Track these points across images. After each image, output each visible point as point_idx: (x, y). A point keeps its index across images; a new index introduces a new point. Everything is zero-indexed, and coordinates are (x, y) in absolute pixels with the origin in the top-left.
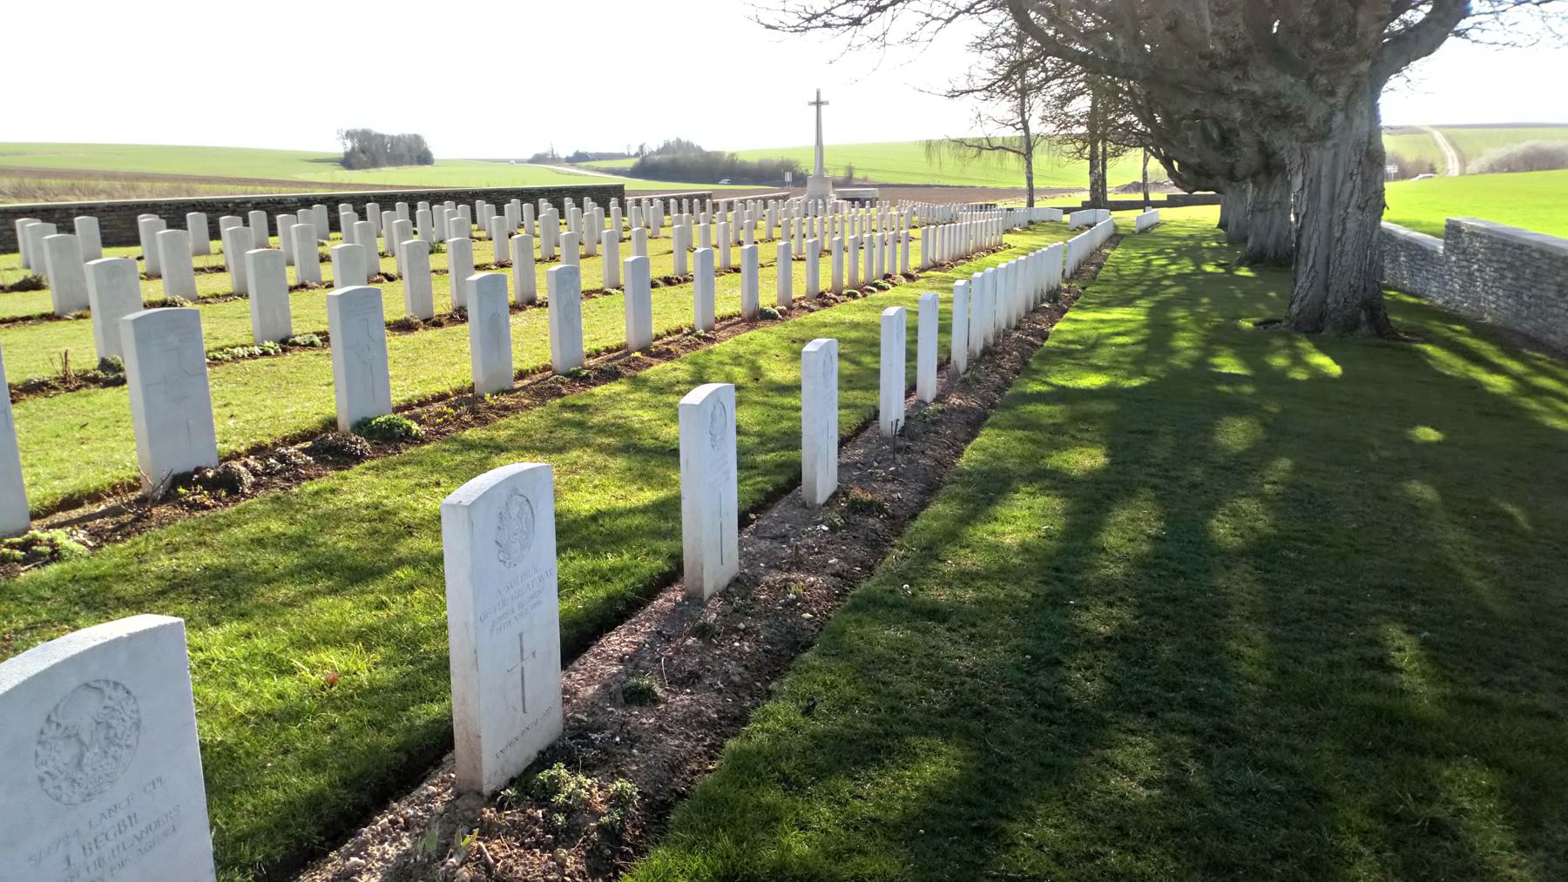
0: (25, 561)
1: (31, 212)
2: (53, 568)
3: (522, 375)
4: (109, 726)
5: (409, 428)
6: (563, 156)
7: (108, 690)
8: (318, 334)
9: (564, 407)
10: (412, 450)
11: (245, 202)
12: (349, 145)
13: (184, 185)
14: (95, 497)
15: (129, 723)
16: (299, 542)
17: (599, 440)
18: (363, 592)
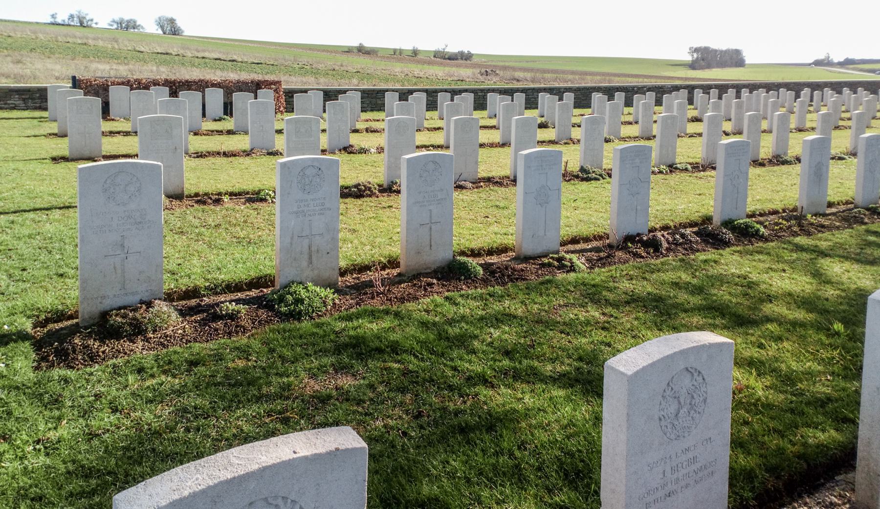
0: (559, 268)
1: (545, 90)
2: (572, 275)
3: (830, 205)
4: (693, 397)
5: (758, 230)
6: (836, 61)
7: (696, 374)
8: (690, 164)
9: (868, 232)
10: (761, 244)
12: (695, 55)
13: (607, 78)
14: (587, 240)
15: (701, 399)
16: (698, 290)
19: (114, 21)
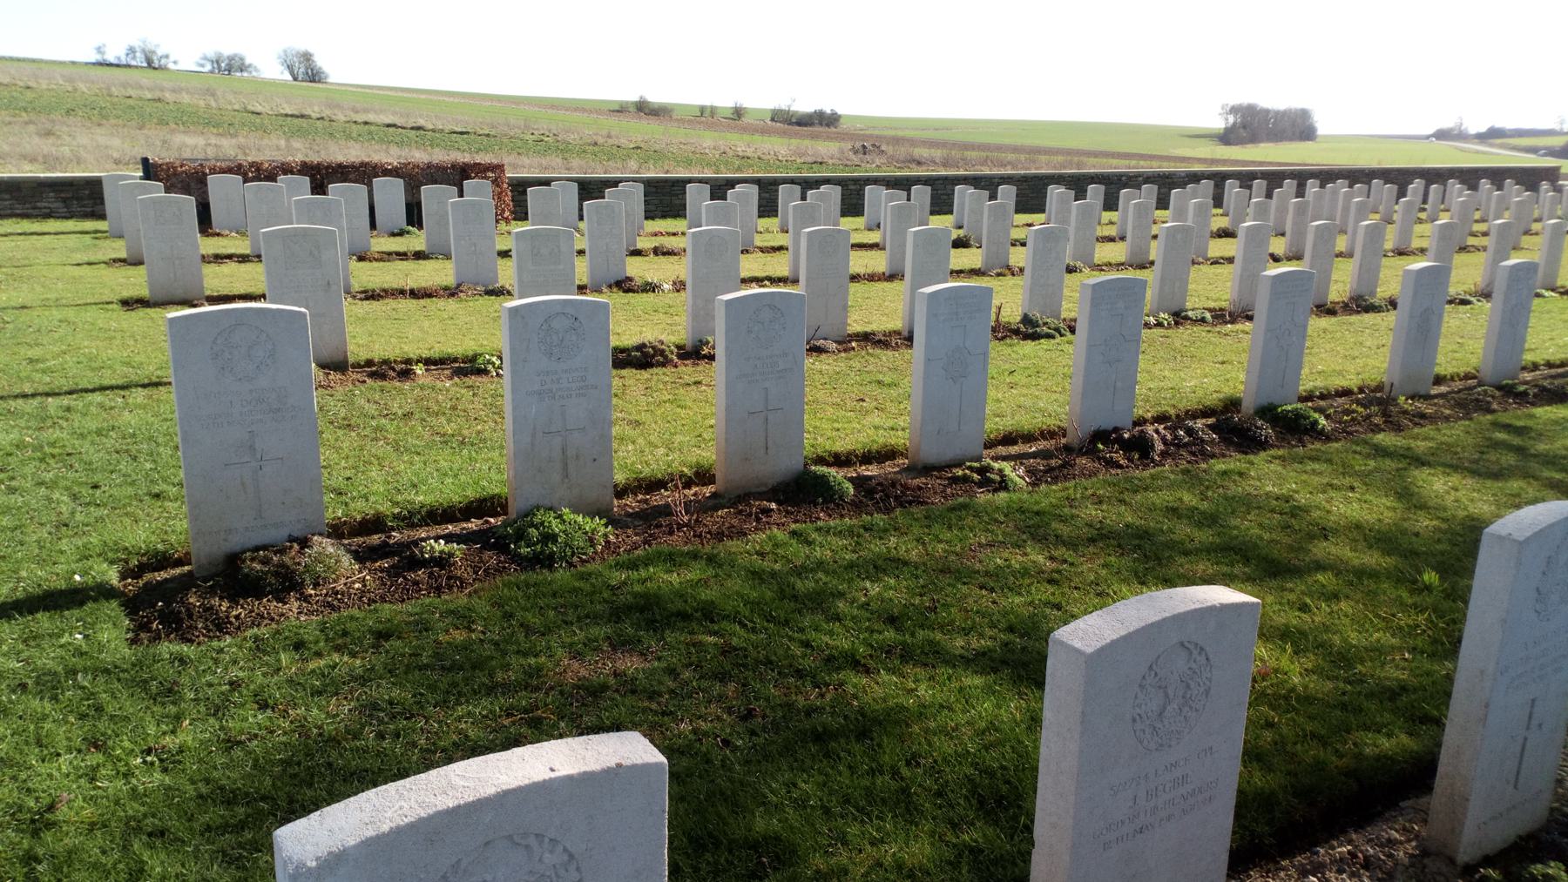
0: (980, 485)
2: (1003, 495)
3: (1439, 380)
4: (1188, 686)
5: (1316, 422)
6: (1472, 131)
8: (1210, 310)
10: (1318, 445)
11: (1139, 175)
12: (1231, 119)
14: (1029, 438)
16: (1209, 520)
17: (1547, 473)
18: (1284, 590)
19: (205, 58)
